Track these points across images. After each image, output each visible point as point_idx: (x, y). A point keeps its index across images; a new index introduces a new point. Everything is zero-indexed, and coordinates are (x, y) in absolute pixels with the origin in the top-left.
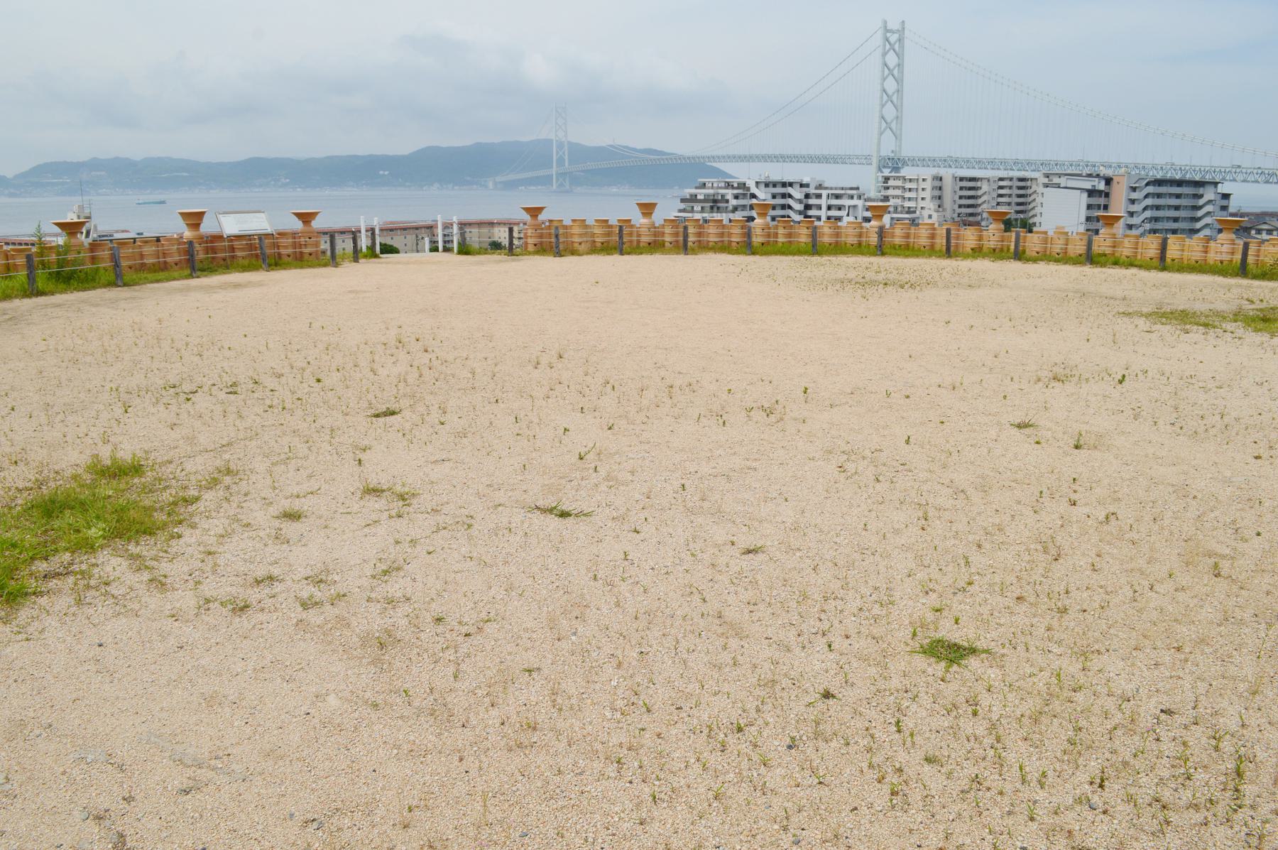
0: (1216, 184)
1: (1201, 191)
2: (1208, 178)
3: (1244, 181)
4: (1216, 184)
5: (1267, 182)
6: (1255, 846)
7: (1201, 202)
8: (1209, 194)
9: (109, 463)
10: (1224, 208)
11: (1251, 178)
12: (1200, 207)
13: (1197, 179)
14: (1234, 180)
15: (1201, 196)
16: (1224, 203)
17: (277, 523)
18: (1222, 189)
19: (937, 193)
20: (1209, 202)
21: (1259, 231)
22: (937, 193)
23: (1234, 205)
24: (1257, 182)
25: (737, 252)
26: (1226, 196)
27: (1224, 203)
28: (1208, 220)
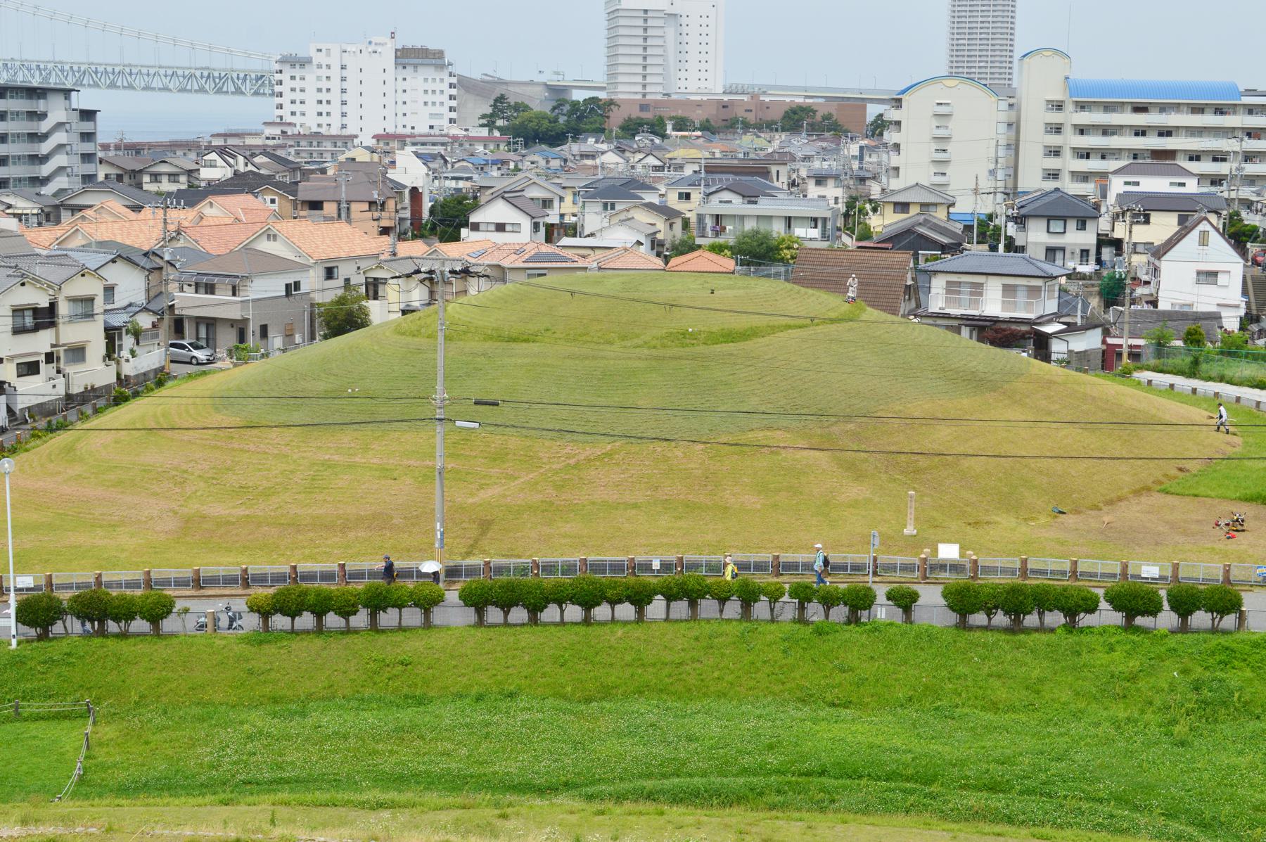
0: (67, 93)
1: (41, 105)
2: (53, 82)
3: (147, 88)
4: (67, 93)
5: (183, 90)
6: (1265, 583)
7: (44, 126)
8: (57, 111)
9: (546, 109)
10: (87, 137)
11: (156, 83)
12: (44, 137)
13: (35, 84)
14: (131, 87)
15: (43, 116)
16: (87, 127)
17: (272, 808)
18: (82, 100)
19: (683, 57)
20: (60, 125)
21: (156, 177)
22: (683, 57)
23: (106, 130)
24: (166, 89)
25: (144, 144)
26: (88, 115)
27: (87, 127)
28: (60, 160)
